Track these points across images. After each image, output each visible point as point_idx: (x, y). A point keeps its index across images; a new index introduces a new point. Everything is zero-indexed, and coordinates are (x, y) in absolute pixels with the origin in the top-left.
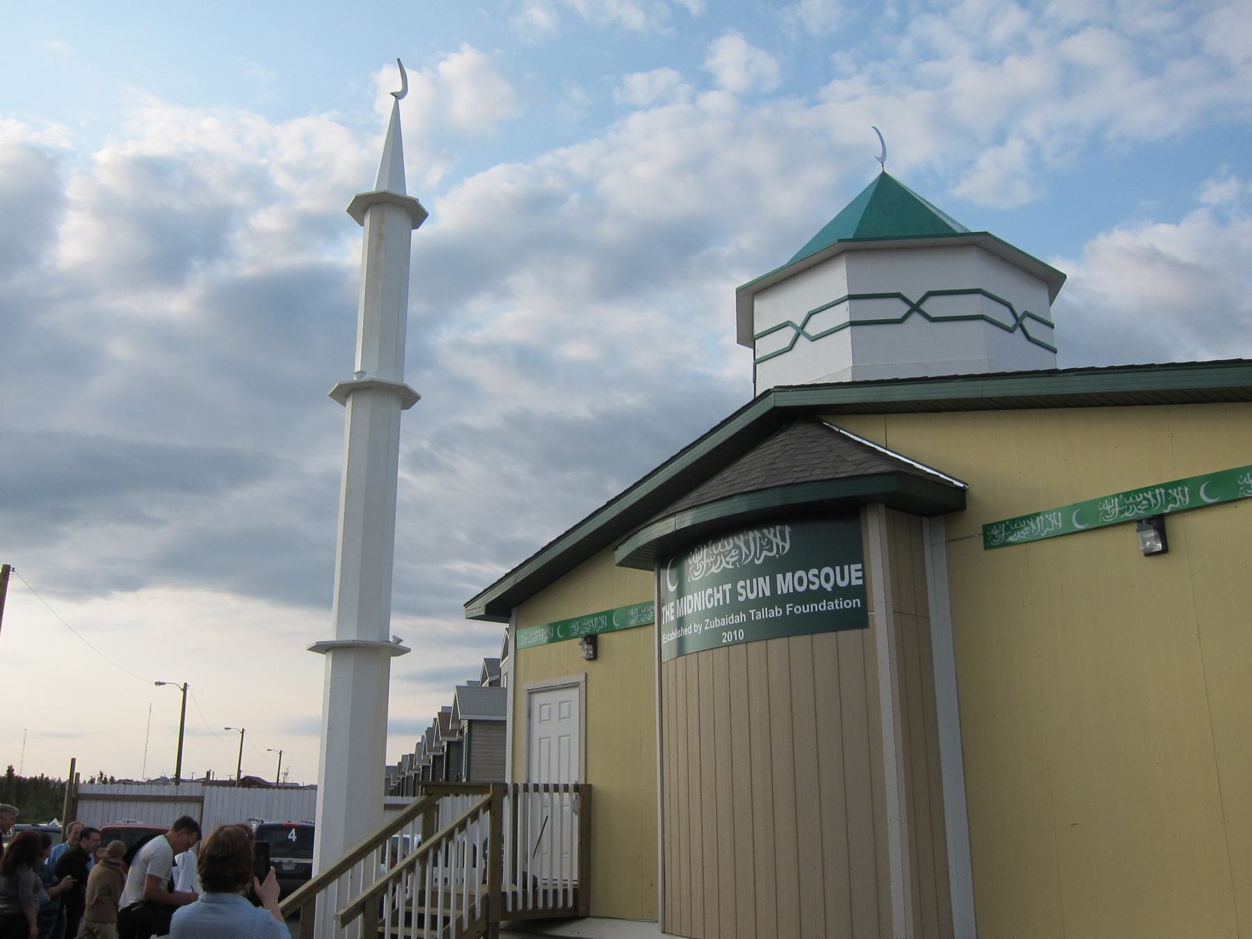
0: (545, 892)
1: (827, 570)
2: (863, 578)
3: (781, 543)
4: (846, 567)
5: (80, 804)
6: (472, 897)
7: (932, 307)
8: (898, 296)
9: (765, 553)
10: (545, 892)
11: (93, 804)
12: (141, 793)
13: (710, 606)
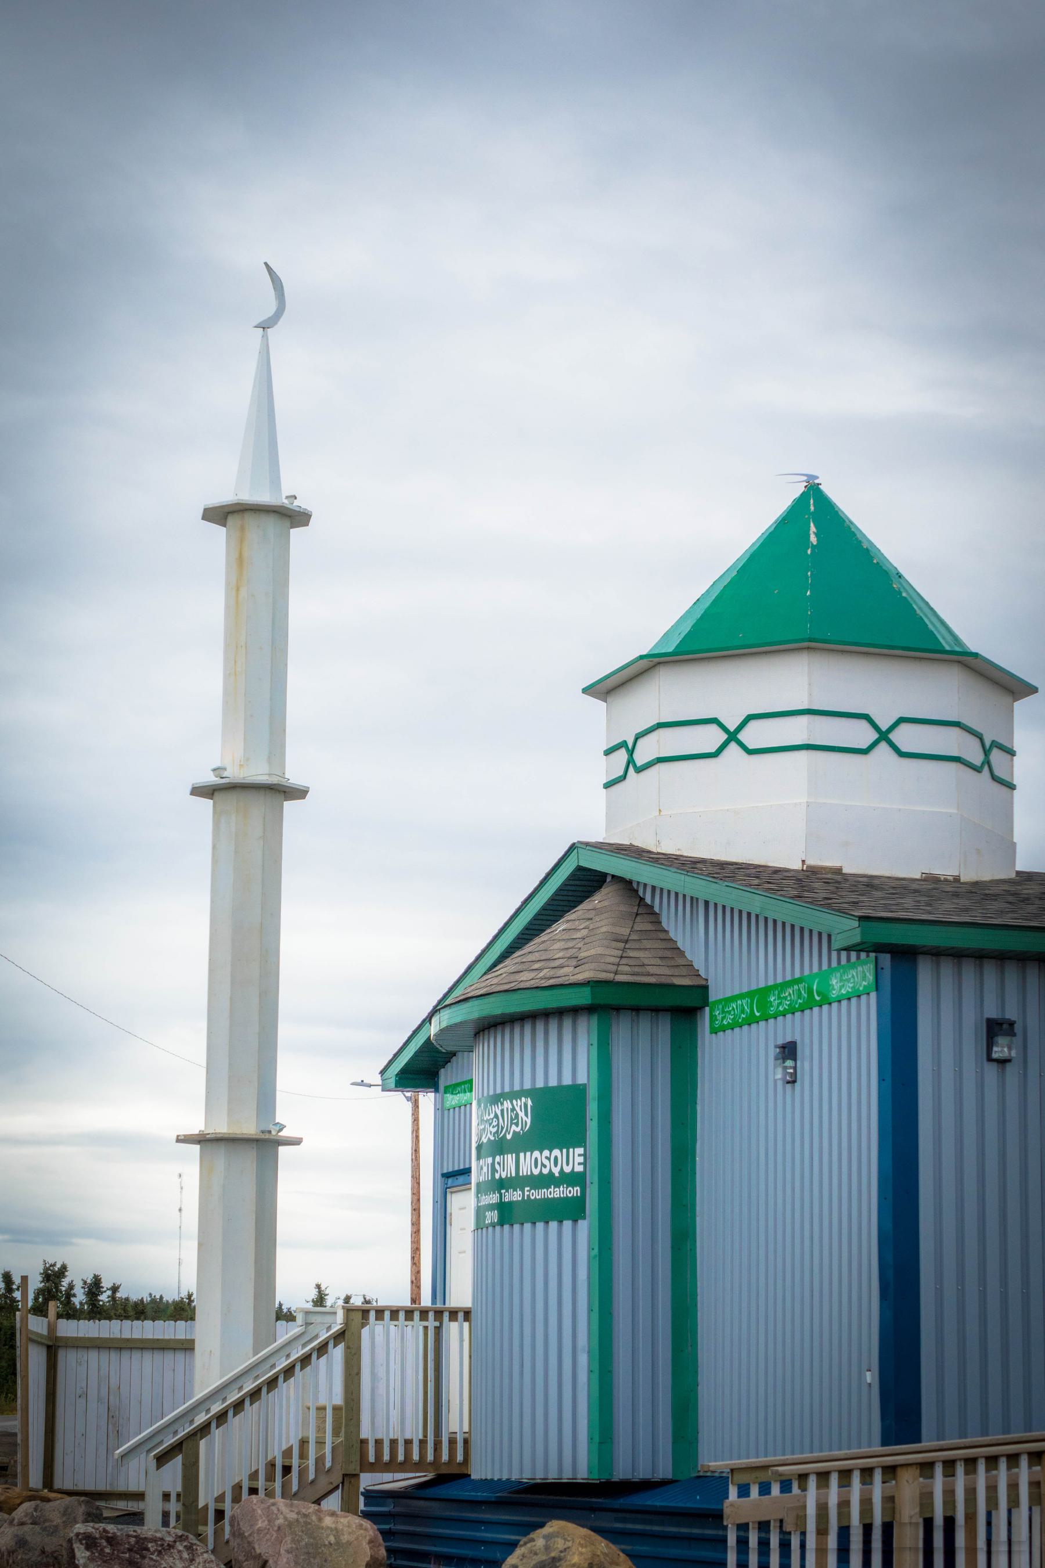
0: (452, 1442)
1: (556, 1152)
2: (585, 1164)
3: (525, 1118)
4: (571, 1150)
5: (61, 1354)
6: (320, 1443)
7: (752, 736)
8: (714, 721)
9: (514, 1127)
10: (452, 1442)
11: (82, 1355)
12: (159, 1336)
13: (536, 1172)
